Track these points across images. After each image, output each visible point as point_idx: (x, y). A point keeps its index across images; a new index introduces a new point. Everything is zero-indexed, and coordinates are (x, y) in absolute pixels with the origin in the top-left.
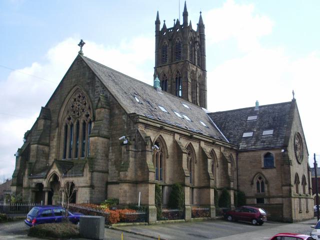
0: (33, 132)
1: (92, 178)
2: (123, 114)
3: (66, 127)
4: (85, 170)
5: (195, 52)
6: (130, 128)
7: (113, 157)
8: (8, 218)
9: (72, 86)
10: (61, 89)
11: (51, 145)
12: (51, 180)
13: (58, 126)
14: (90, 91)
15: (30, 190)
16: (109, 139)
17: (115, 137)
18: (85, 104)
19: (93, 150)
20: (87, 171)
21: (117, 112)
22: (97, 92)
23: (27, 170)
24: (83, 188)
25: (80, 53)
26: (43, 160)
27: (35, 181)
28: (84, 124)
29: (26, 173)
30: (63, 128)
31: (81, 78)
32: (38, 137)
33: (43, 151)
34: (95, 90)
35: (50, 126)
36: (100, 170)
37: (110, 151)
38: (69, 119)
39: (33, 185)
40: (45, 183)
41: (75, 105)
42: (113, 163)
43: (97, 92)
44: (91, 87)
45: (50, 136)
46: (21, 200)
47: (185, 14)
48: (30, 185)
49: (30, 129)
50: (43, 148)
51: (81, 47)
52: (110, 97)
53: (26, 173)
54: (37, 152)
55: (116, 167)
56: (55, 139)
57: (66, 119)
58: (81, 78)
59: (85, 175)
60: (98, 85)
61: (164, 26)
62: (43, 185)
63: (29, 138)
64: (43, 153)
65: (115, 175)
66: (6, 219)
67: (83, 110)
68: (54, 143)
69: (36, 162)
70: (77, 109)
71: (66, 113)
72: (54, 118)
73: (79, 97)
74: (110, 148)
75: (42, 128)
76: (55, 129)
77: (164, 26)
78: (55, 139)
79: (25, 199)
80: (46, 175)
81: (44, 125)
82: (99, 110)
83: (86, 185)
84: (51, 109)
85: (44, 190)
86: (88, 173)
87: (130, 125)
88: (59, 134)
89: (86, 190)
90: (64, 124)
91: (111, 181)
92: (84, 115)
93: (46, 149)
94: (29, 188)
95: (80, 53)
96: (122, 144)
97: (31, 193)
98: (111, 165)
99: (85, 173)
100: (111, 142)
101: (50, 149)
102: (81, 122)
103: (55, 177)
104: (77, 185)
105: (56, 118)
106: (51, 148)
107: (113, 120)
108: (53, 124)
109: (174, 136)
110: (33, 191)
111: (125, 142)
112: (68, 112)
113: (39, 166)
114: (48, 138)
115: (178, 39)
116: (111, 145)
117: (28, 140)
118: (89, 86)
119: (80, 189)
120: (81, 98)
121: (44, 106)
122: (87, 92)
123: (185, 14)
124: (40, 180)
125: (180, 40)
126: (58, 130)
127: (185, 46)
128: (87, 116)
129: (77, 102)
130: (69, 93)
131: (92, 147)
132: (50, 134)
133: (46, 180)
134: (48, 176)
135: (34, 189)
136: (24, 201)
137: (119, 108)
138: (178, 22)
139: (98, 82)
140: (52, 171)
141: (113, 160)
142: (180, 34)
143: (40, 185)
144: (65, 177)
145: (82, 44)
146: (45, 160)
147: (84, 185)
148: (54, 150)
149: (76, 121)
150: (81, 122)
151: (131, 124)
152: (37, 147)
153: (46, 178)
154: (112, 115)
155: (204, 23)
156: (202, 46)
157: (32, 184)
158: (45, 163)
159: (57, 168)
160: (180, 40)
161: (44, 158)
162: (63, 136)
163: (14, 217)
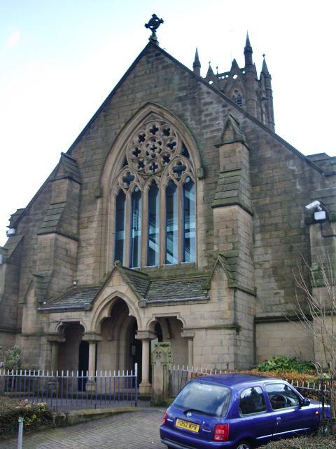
0: (32, 212)
1: (234, 306)
2: (288, 158)
3: (121, 197)
4: (214, 284)
5: (262, 115)
6: (314, 189)
7: (269, 257)
8: (55, 415)
9: (137, 106)
10: (105, 116)
11: (82, 237)
12: (106, 314)
13: (100, 196)
14: (188, 114)
15: (44, 340)
16: (252, 215)
17: (269, 212)
18: (171, 146)
19: (227, 237)
20: (219, 287)
21: (269, 153)
22: (207, 115)
23: (32, 292)
24: (209, 332)
25: (153, 42)
26: (65, 270)
27: (58, 317)
28: (170, 190)
29: (32, 299)
30: (113, 200)
31: (161, 89)
32: (58, 217)
33: (67, 251)
34: (201, 112)
35: (80, 197)
36: (245, 286)
37: (258, 243)
38: (128, 180)
39: (54, 329)
40: (89, 323)
41: (144, 149)
42: (270, 271)
43: (207, 115)
44: (189, 107)
45: (79, 219)
46: (19, 363)
47: (248, 51)
48: (42, 328)
49: (24, 206)
50: (66, 243)
51: (154, 30)
52: (245, 122)
53: (32, 299)
54: (55, 251)
55: (276, 281)
56: (95, 225)
57: (120, 180)
58: (161, 89)
59: (214, 299)
60: (208, 100)
61: (210, 71)
62: (82, 328)
63: (21, 225)
64: (67, 255)
65: (277, 299)
66: (50, 418)
67: (166, 159)
68: (91, 233)
69: (52, 276)
70: (150, 157)
71: (119, 167)
72: (90, 179)
73: (154, 130)
74: (258, 237)
75: (63, 198)
76: (93, 202)
77: (210, 71)
78: (95, 225)
79: (27, 361)
80: (93, 303)
81: (69, 192)
82: (227, 148)
83: (221, 323)
84: (81, 161)
85: (85, 338)
86: (224, 292)
87: (311, 182)
88: (104, 214)
89: (221, 337)
90: (116, 192)
91: (264, 315)
92: (169, 168)
93: (72, 246)
94: (39, 334)
95: (153, 42)
96: (311, 221)
97: (46, 347)
98: (263, 277)
99: (214, 293)
100: (258, 223)
101: (79, 247)
102: (163, 183)
103: (119, 306)
104: (187, 323)
105: (95, 179)
106: (83, 244)
107: (260, 171)
108: (85, 192)
109: (256, 247)
110: (51, 343)
111: (320, 215)
112: (125, 163)
113: (60, 284)
114: (75, 222)
115: (236, 91)
116: (258, 229)
117: (19, 231)
118: (184, 105)
119: (199, 335)
120: (159, 134)
121: (65, 152)
122: (181, 117)
123: (248, 51)
124: (74, 316)
125: (240, 92)
126: (102, 203)
127: (250, 102)
128: (179, 170)
129: (150, 143)
130: (133, 117)
131: (222, 231)
132: (79, 213)
133: (92, 314)
134: (97, 304)
135: (55, 338)
136: (25, 365)
137: (275, 146)
138: (234, 64)
139: (208, 93)
140: (108, 292)
141: (267, 265)
142: (240, 83)
143: (72, 329)
144: (147, 306)
145: (154, 23)
146: (70, 273)
147: (213, 323)
148: (92, 249)
149: (149, 183)
150: (163, 183)
151: (314, 180)
152: (56, 239)
153: (91, 310)
154: (255, 162)
155: (270, 72)
156: (270, 108)
157: (49, 324)
158: (69, 279)
159: (122, 283)
160: (240, 92)
161: (68, 266)
162: (112, 218)
163: (73, 413)
